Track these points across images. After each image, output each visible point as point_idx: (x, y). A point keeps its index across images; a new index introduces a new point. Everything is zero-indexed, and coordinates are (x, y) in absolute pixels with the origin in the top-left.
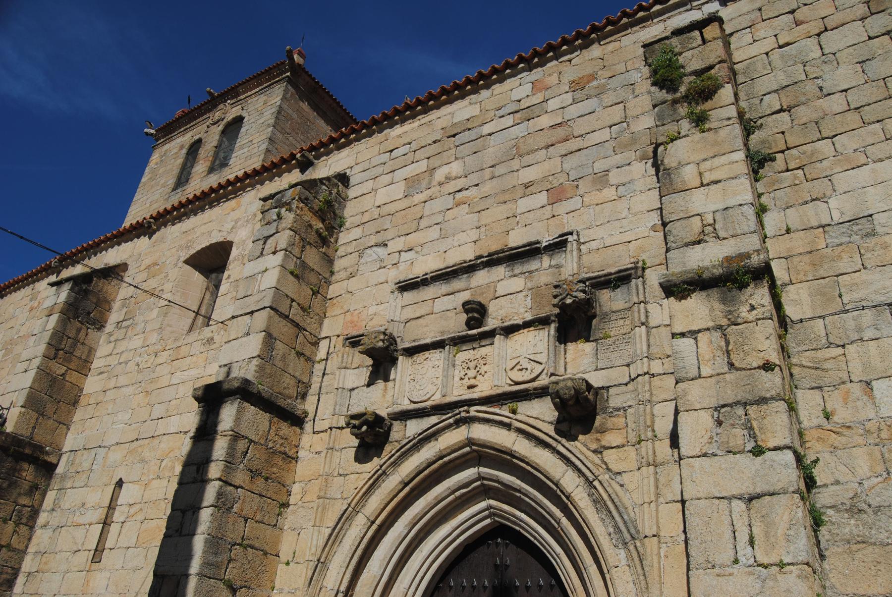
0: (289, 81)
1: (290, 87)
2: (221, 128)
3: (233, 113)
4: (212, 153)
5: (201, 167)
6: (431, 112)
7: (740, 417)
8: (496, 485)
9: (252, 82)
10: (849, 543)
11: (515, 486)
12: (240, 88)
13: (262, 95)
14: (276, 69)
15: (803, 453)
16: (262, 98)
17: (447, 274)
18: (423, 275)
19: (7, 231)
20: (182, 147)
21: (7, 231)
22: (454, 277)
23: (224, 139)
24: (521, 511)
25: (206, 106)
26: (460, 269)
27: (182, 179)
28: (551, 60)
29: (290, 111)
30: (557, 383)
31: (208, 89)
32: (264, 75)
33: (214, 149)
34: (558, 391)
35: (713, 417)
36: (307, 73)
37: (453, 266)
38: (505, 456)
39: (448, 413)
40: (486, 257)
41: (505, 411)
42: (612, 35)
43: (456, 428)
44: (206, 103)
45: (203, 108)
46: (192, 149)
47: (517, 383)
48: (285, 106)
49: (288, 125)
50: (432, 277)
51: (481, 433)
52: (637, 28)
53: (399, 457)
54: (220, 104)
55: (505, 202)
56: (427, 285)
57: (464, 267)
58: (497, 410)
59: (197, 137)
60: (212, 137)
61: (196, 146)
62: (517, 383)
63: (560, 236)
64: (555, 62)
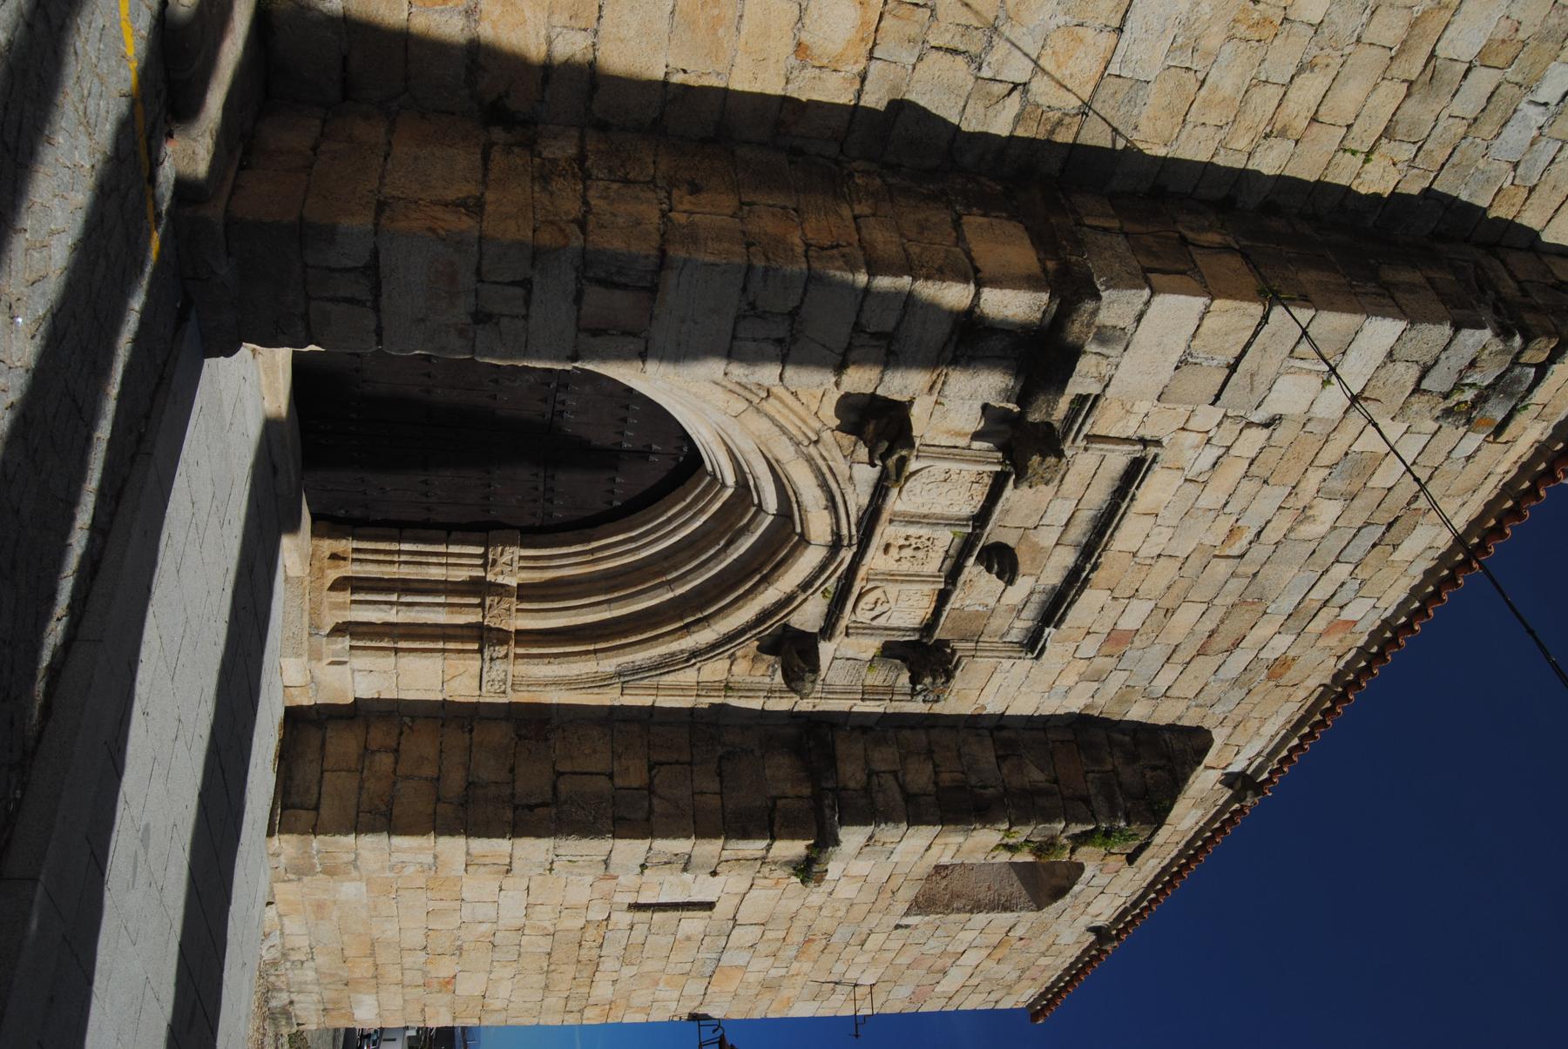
6: (1496, 492)
8: (745, 521)
11: (732, 547)
17: (1106, 525)
18: (1134, 495)
19: (1547, 655)
21: (1547, 655)
22: (1095, 527)
24: (705, 522)
26: (1098, 543)
28: (1368, 644)
30: (814, 682)
34: (803, 680)
37: (1112, 534)
38: (768, 569)
39: (858, 531)
40: (1088, 575)
41: (831, 584)
42: (1318, 699)
43: (832, 531)
47: (860, 596)
50: (1119, 507)
51: (810, 559)
52: (1296, 718)
53: (819, 469)
55: (1168, 588)
56: (1115, 492)
57: (1095, 549)
58: (834, 579)
62: (860, 596)
63: (1044, 647)
64: (1361, 643)
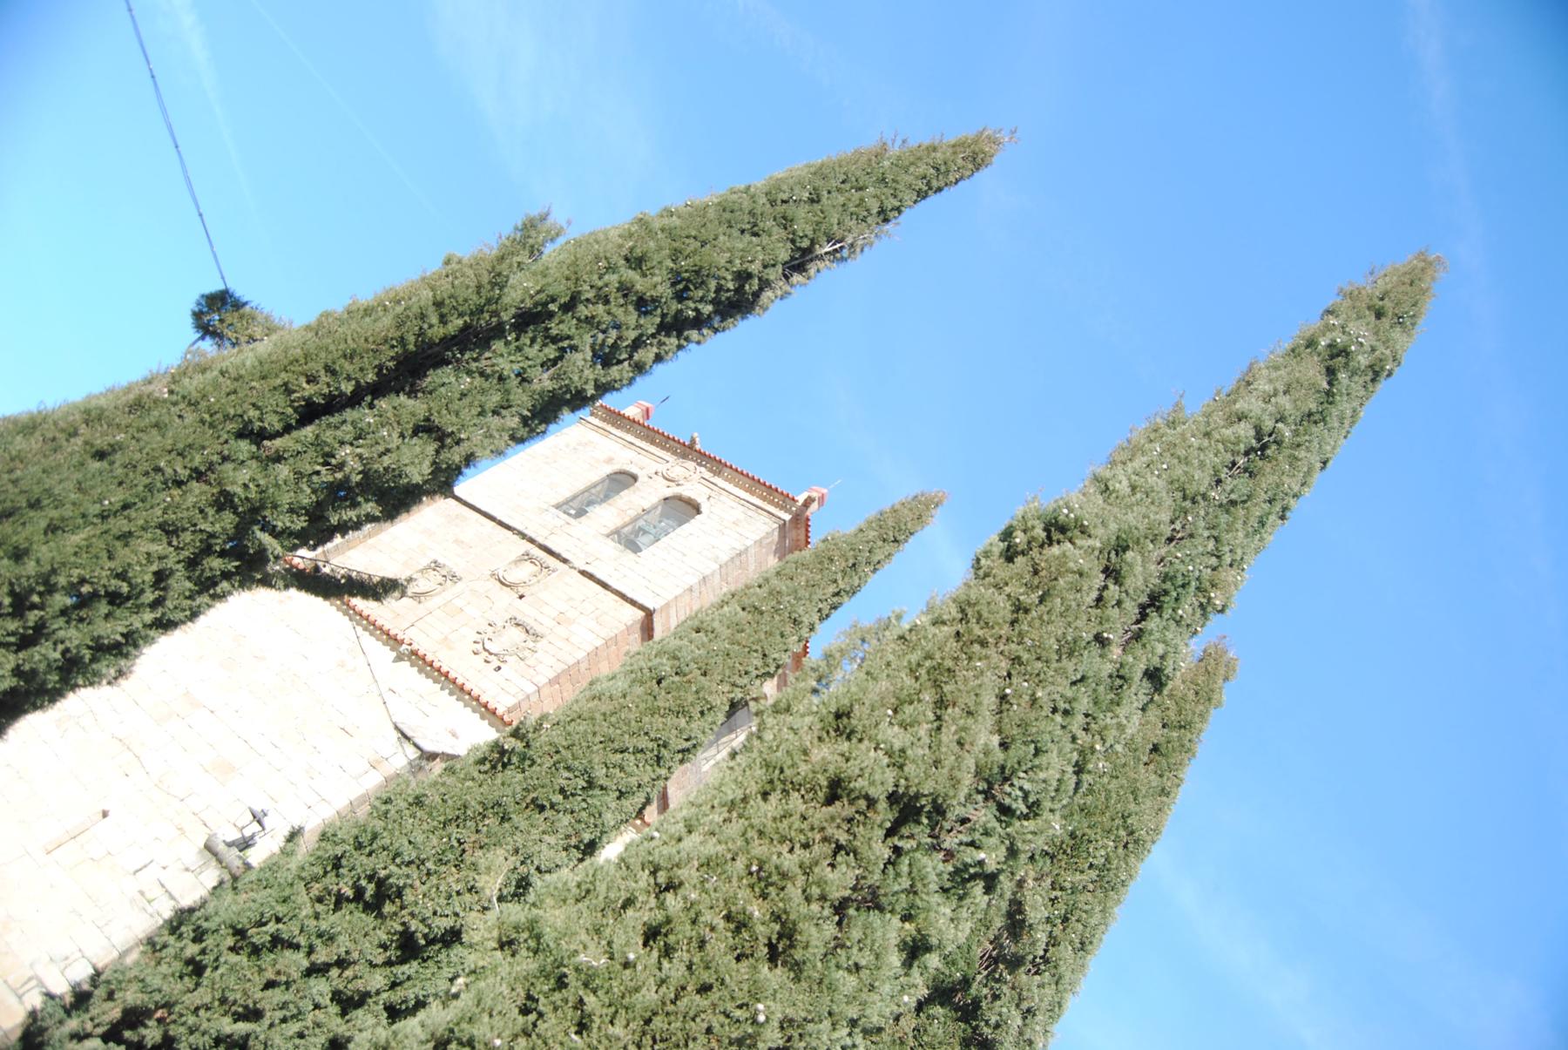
0: (783, 527)
1: (776, 533)
2: (669, 493)
3: (695, 490)
4: (632, 513)
5: (608, 515)
7: (541, 757)
9: (746, 479)
10: (812, 201)
12: (728, 470)
13: (742, 508)
14: (782, 498)
15: (513, 311)
16: (739, 512)
20: (610, 461)
23: (660, 508)
25: (676, 445)
27: (577, 506)
29: (752, 560)
31: (696, 435)
32: (763, 488)
33: (640, 511)
35: (688, 795)
36: (807, 531)
44: (679, 442)
45: (671, 442)
46: (619, 477)
48: (752, 551)
49: (736, 574)
54: (692, 460)
59: (634, 470)
60: (648, 494)
61: (623, 480)
